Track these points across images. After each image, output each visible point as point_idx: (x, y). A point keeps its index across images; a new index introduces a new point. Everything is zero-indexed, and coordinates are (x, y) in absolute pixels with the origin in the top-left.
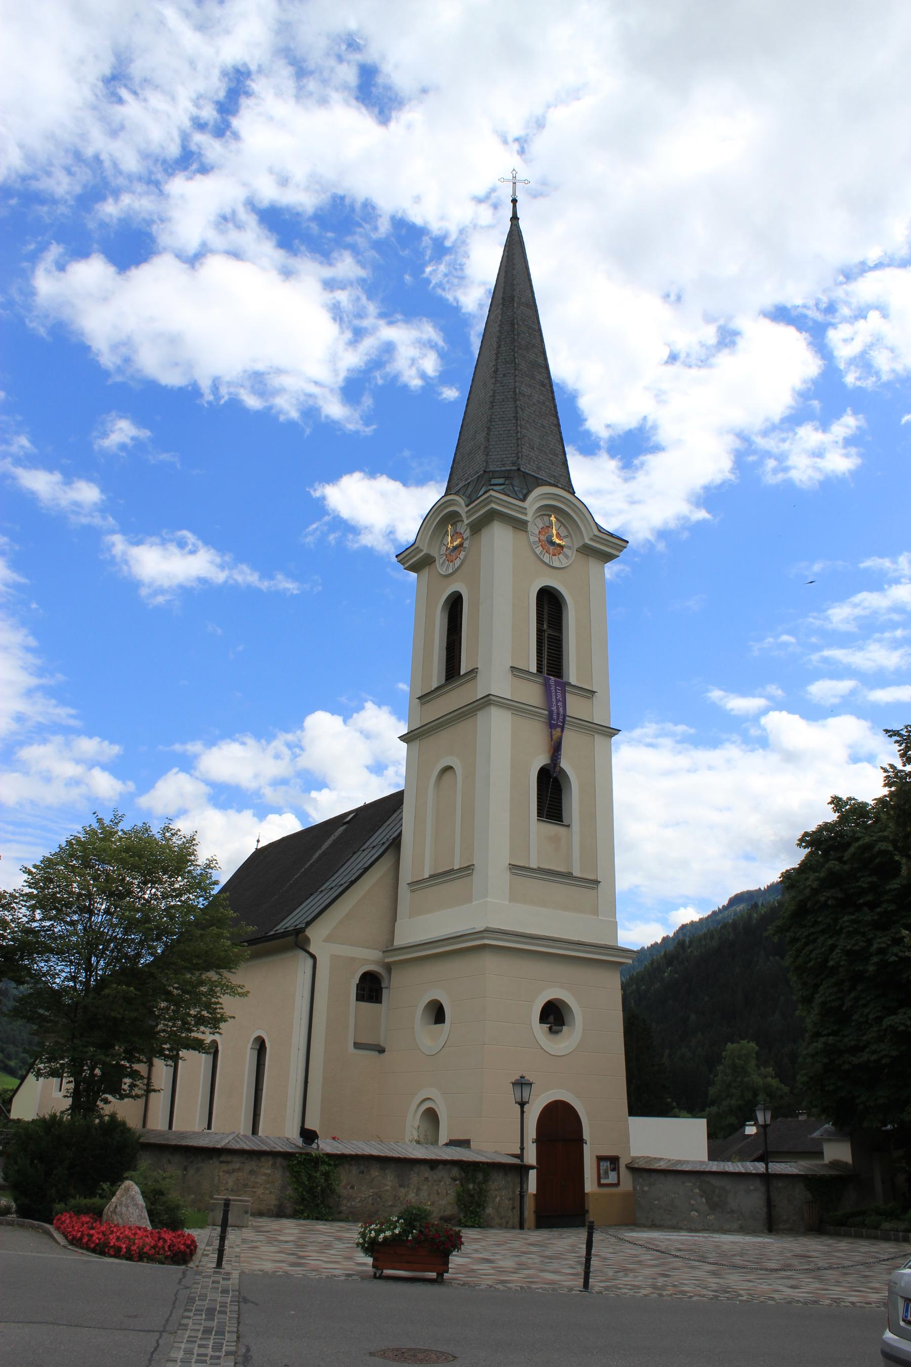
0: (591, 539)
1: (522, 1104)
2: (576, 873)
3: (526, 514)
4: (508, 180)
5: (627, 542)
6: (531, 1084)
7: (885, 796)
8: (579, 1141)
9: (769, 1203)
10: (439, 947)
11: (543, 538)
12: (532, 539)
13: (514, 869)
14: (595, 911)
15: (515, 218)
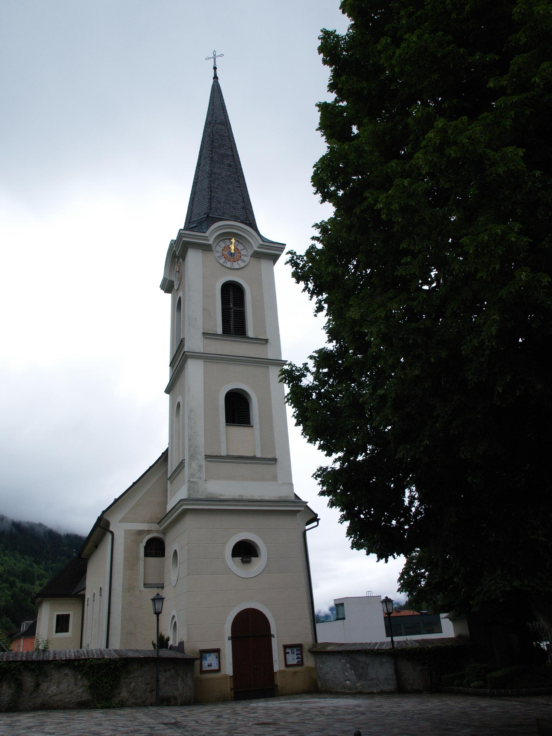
0: (258, 247)
1: (158, 614)
2: (259, 455)
3: (208, 240)
4: (211, 58)
5: (285, 245)
6: (163, 599)
7: (289, 387)
8: (269, 636)
9: (396, 671)
10: (173, 514)
11: (226, 253)
12: (217, 255)
13: (208, 458)
14: (274, 478)
15: (216, 78)
